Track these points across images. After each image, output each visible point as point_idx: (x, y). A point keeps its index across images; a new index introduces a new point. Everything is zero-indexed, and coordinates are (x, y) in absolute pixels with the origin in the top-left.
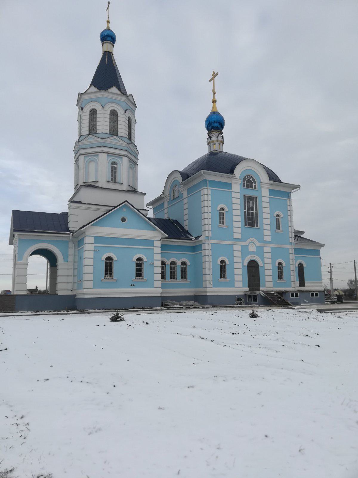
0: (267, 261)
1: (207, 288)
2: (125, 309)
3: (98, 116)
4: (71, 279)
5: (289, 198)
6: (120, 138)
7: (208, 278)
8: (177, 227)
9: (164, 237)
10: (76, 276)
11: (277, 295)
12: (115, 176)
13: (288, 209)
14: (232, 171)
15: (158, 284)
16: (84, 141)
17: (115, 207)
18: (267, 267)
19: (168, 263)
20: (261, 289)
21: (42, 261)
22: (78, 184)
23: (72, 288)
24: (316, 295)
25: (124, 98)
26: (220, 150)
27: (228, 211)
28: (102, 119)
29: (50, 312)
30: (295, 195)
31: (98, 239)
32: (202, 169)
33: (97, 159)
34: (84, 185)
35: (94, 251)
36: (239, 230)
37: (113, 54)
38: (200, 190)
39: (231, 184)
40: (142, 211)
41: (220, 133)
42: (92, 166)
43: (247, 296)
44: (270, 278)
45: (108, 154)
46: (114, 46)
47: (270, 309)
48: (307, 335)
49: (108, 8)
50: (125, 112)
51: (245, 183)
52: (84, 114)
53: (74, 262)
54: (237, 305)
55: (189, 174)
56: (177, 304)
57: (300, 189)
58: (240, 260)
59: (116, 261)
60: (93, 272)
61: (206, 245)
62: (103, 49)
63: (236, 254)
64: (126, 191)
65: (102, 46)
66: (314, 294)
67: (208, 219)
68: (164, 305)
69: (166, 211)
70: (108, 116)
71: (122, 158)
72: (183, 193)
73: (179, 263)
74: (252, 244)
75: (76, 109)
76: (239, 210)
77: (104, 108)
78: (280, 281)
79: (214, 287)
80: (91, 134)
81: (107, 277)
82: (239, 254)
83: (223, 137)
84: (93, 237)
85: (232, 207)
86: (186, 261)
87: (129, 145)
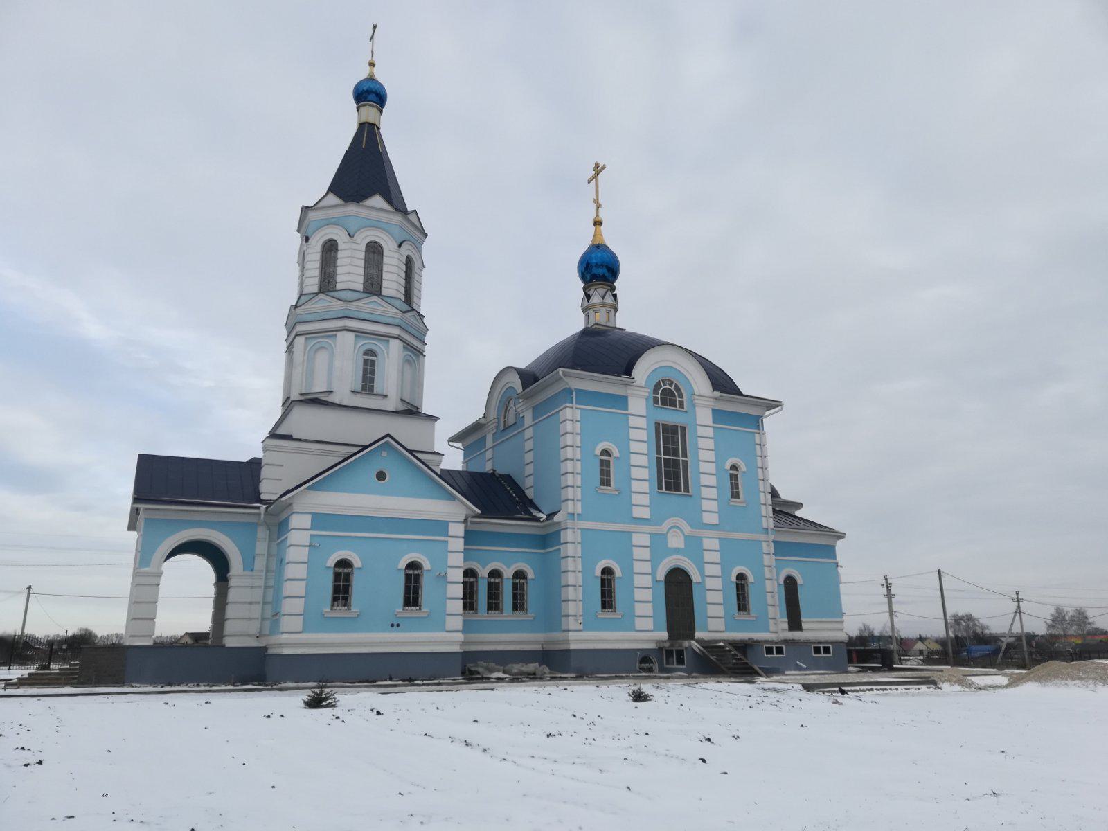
0: (709, 570)
1: (571, 633)
2: (368, 682)
3: (340, 254)
4: (256, 611)
5: (759, 429)
6: (389, 300)
7: (572, 608)
8: (509, 492)
9: (473, 514)
10: (269, 603)
11: (730, 651)
12: (372, 380)
13: (756, 453)
14: (628, 371)
15: (456, 622)
16: (308, 306)
17: (365, 447)
18: (711, 583)
19: (483, 572)
20: (698, 635)
21: (199, 570)
22: (288, 398)
23: (258, 630)
24: (827, 650)
25: (397, 218)
26: (609, 324)
27: (619, 456)
28: (348, 261)
29: (198, 685)
30: (771, 421)
31: (320, 520)
32: (560, 367)
33: (332, 344)
34: (301, 401)
35: (310, 546)
36: (645, 500)
37: (379, 129)
38: (557, 410)
39: (627, 397)
40: (420, 456)
41: (609, 288)
42: (322, 358)
43: (664, 652)
44: (719, 611)
45: (358, 334)
46: (381, 112)
47: (697, 684)
48: (709, 740)
49: (372, 38)
50: (400, 246)
51: (659, 396)
52: (309, 250)
53: (267, 571)
54: (640, 672)
55: (538, 375)
56: (499, 671)
57: (782, 409)
58: (647, 567)
59: (360, 568)
60: (306, 593)
61: (569, 531)
62: (360, 117)
63: (638, 553)
64: (393, 412)
65: (358, 111)
66: (821, 648)
67: (573, 473)
68: (467, 672)
69: (489, 454)
70: (363, 255)
71: (388, 341)
72: (523, 416)
73: (508, 573)
74: (675, 530)
75: (297, 238)
76: (644, 454)
77: (355, 238)
78: (743, 617)
79: (585, 629)
80: (323, 293)
81: (338, 606)
82: (645, 553)
83: (615, 296)
84: (310, 516)
85: (629, 448)
86: (524, 569)
87: (405, 315)
